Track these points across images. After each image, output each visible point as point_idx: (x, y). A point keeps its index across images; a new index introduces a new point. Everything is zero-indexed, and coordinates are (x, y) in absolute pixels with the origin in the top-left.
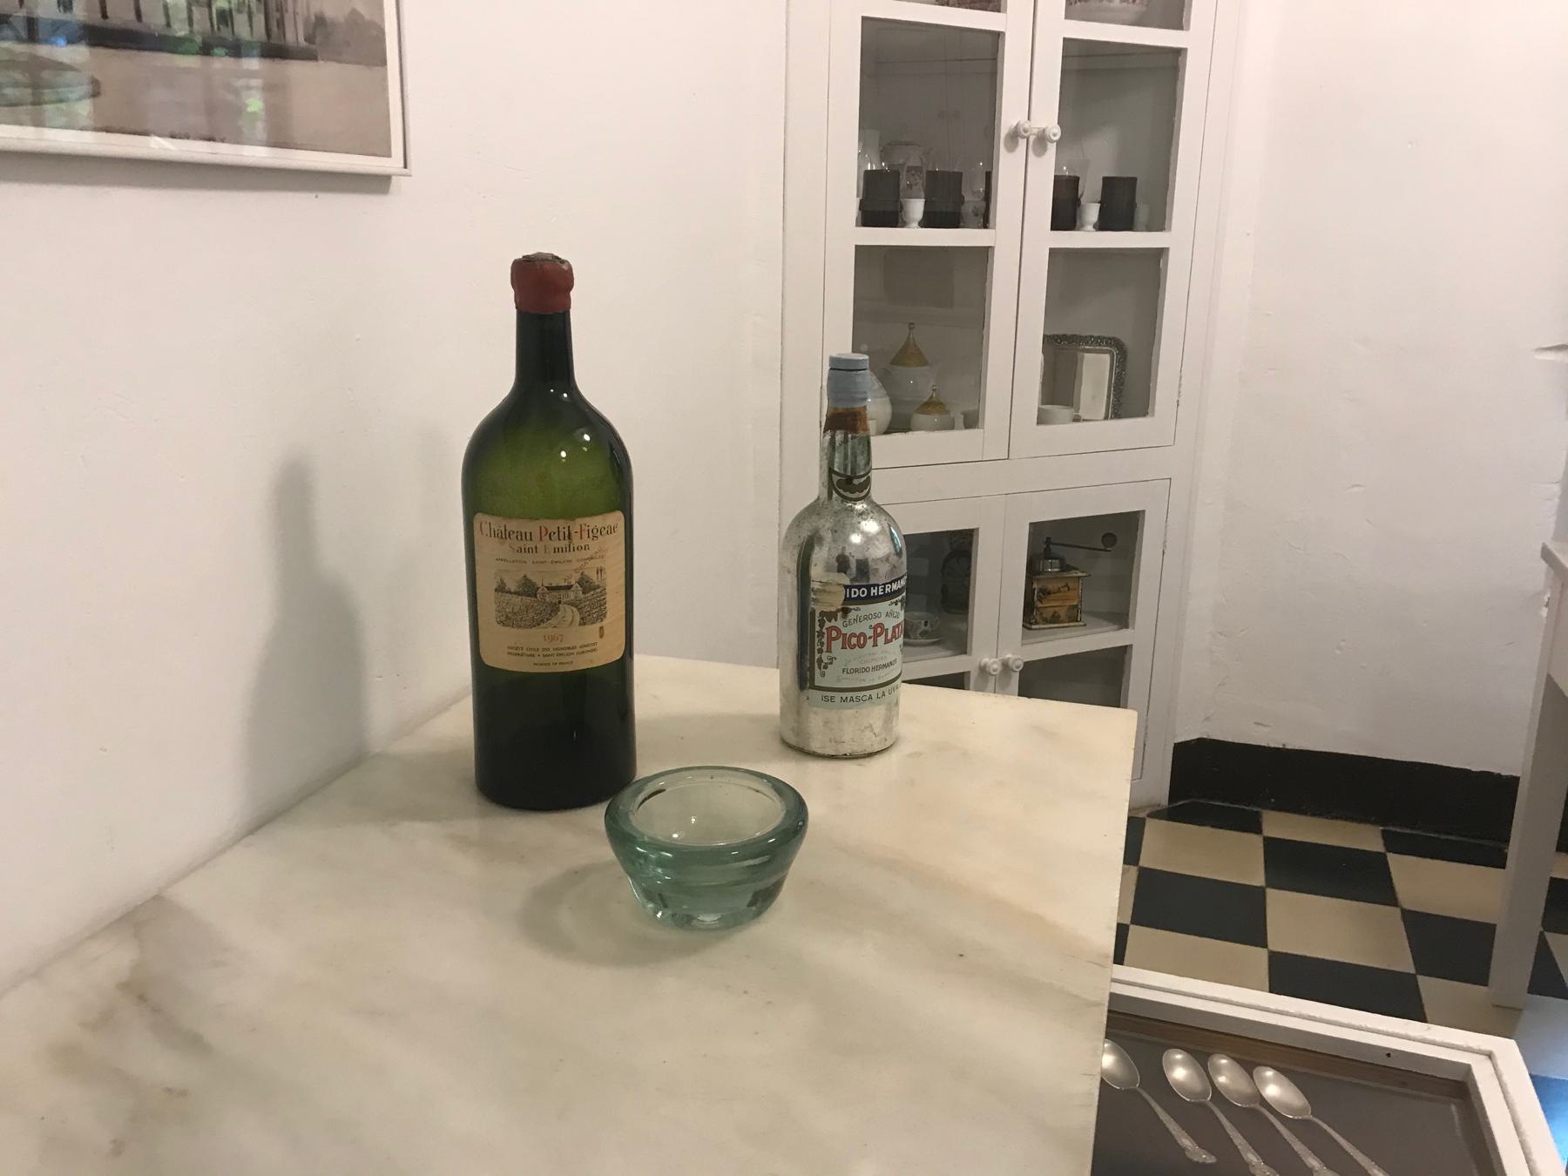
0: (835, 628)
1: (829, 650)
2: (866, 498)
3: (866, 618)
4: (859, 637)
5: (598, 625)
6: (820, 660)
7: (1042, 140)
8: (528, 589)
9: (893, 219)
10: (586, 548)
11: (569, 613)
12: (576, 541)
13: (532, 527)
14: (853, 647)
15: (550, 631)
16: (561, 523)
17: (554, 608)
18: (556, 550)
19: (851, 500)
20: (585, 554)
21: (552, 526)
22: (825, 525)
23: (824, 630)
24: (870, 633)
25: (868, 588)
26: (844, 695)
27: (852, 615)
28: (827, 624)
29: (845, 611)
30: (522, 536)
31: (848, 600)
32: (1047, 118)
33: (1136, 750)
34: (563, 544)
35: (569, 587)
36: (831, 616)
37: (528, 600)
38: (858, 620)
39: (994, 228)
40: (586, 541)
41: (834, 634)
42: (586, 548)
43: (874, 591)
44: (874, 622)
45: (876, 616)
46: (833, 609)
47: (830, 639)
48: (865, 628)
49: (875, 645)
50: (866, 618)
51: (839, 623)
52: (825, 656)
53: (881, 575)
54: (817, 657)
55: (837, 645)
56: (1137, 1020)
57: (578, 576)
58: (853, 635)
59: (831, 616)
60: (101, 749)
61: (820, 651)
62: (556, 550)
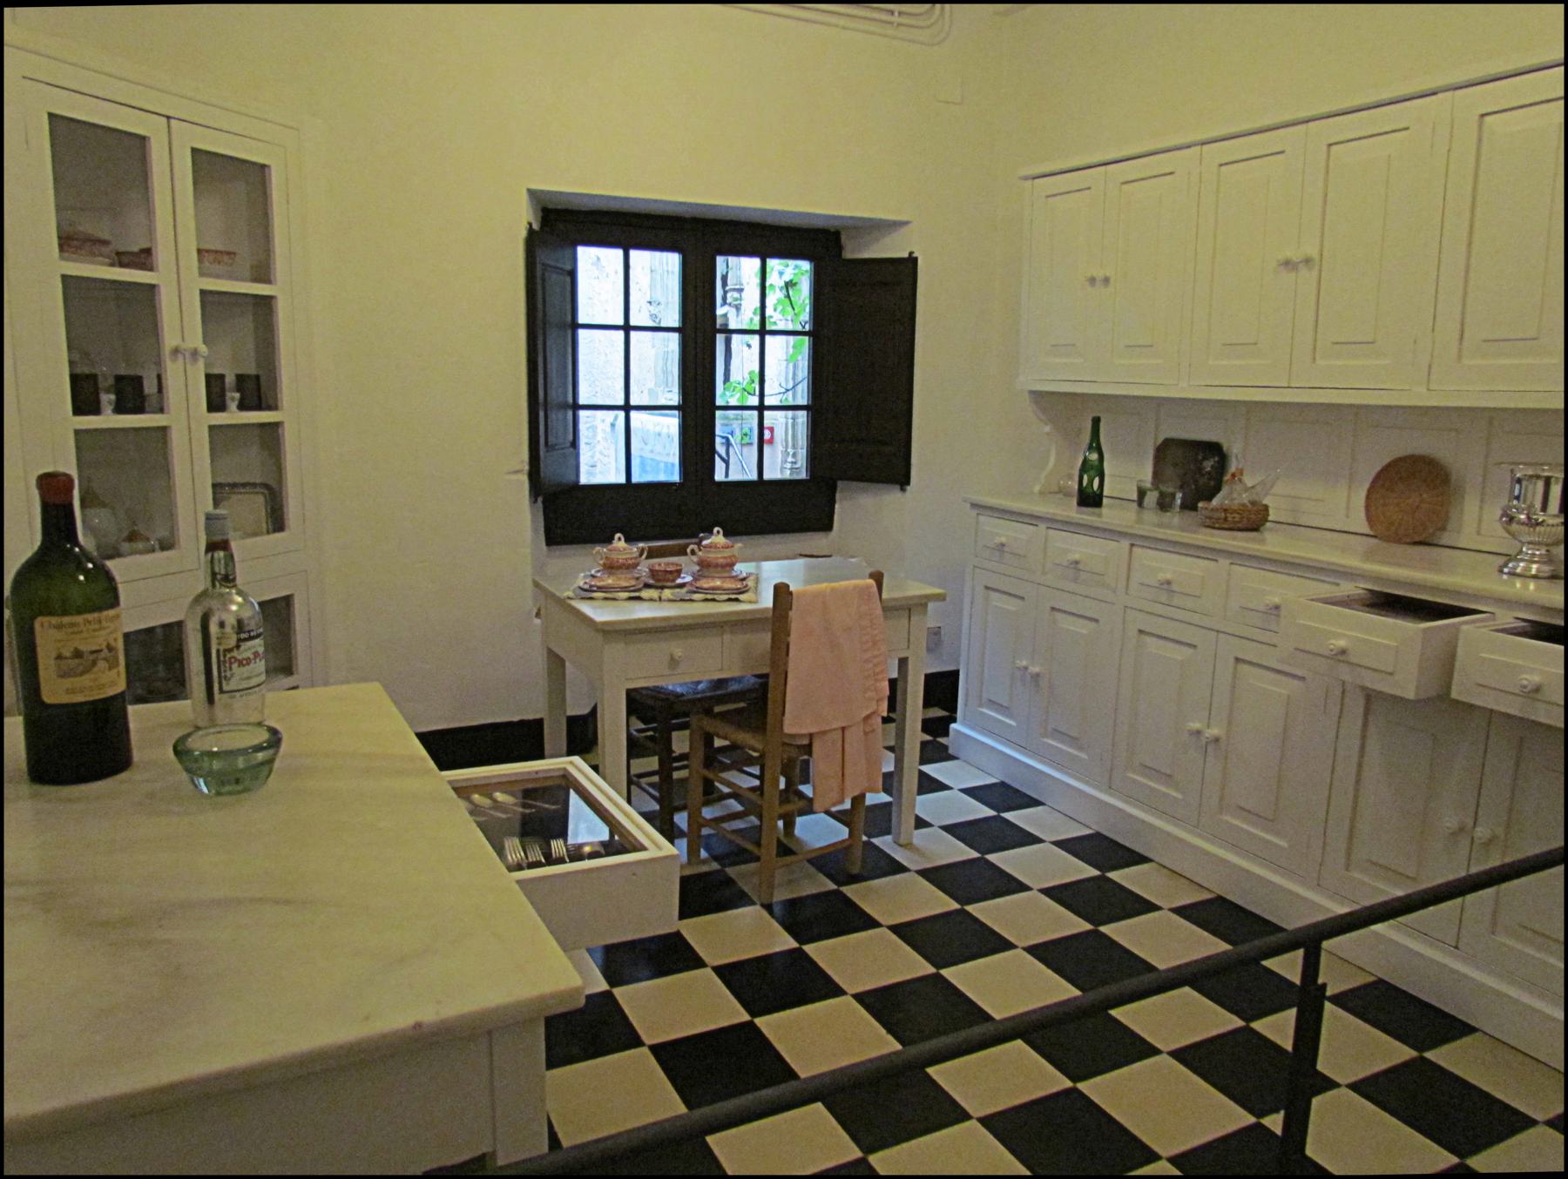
0: (234, 657)
1: (231, 669)
2: (235, 586)
3: (249, 649)
4: (246, 660)
5: (116, 670)
6: (225, 677)
7: (195, 353)
8: (78, 654)
9: (96, 411)
10: (108, 627)
11: (102, 664)
12: (104, 624)
13: (79, 619)
14: (244, 666)
15: (92, 676)
16: (96, 615)
17: (94, 663)
18: (95, 630)
19: (225, 586)
20: (108, 631)
21: (90, 617)
22: (214, 604)
23: (227, 658)
24: (252, 657)
25: (249, 632)
26: (241, 693)
27: (242, 648)
28: (228, 656)
29: (238, 647)
30: (73, 625)
31: (239, 640)
32: (195, 339)
33: (579, 430)
34: (97, 626)
35: (101, 651)
36: (230, 650)
37: (77, 661)
38: (246, 650)
39: (168, 413)
40: (108, 624)
41: (233, 660)
42: (108, 627)
43: (252, 634)
44: (253, 650)
45: (254, 647)
46: (230, 646)
47: (231, 663)
48: (249, 654)
49: (255, 662)
50: (249, 649)
51: (235, 653)
52: (228, 674)
53: (252, 625)
54: (223, 674)
55: (235, 666)
56: (570, 350)
57: (105, 644)
58: (244, 659)
59: (230, 650)
60: (1106, 280)
61: (225, 671)
62: (95, 630)
